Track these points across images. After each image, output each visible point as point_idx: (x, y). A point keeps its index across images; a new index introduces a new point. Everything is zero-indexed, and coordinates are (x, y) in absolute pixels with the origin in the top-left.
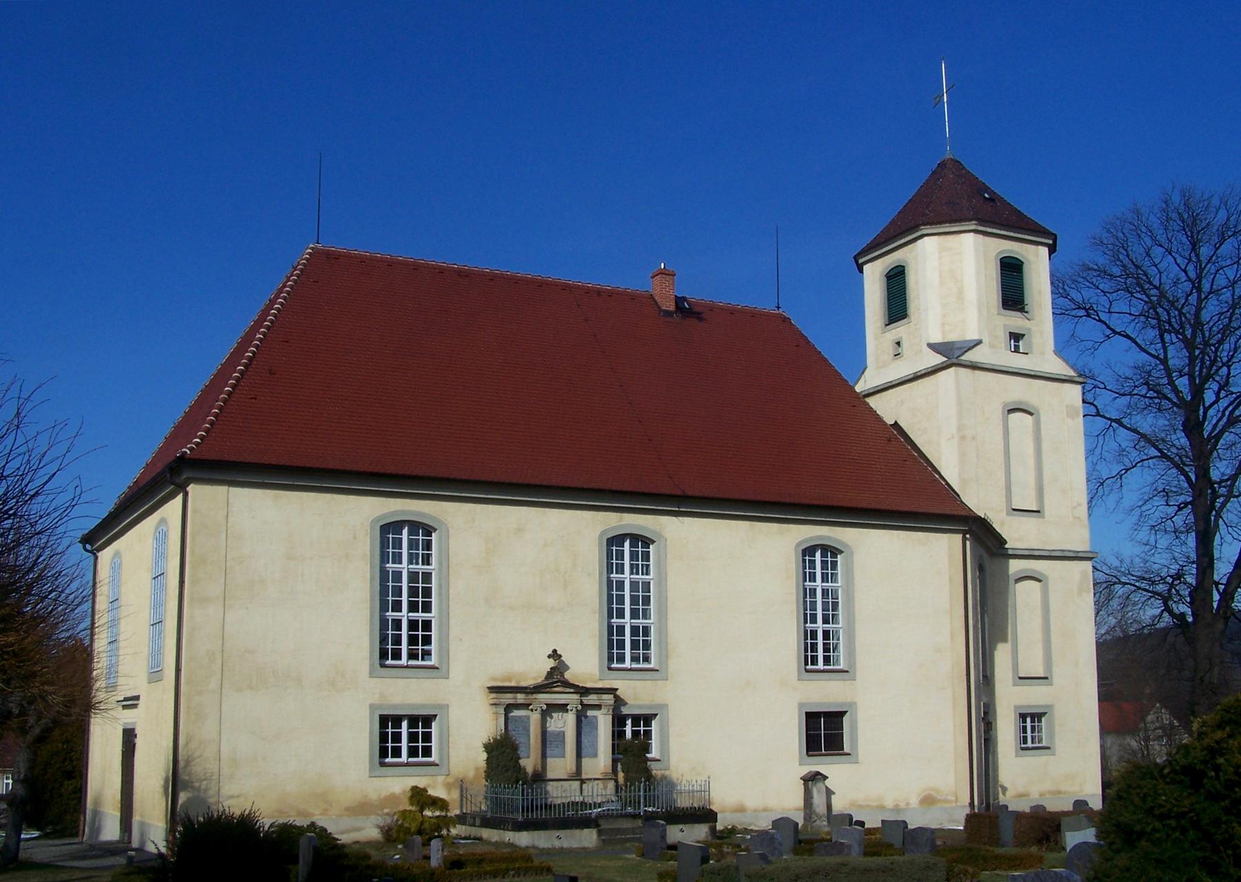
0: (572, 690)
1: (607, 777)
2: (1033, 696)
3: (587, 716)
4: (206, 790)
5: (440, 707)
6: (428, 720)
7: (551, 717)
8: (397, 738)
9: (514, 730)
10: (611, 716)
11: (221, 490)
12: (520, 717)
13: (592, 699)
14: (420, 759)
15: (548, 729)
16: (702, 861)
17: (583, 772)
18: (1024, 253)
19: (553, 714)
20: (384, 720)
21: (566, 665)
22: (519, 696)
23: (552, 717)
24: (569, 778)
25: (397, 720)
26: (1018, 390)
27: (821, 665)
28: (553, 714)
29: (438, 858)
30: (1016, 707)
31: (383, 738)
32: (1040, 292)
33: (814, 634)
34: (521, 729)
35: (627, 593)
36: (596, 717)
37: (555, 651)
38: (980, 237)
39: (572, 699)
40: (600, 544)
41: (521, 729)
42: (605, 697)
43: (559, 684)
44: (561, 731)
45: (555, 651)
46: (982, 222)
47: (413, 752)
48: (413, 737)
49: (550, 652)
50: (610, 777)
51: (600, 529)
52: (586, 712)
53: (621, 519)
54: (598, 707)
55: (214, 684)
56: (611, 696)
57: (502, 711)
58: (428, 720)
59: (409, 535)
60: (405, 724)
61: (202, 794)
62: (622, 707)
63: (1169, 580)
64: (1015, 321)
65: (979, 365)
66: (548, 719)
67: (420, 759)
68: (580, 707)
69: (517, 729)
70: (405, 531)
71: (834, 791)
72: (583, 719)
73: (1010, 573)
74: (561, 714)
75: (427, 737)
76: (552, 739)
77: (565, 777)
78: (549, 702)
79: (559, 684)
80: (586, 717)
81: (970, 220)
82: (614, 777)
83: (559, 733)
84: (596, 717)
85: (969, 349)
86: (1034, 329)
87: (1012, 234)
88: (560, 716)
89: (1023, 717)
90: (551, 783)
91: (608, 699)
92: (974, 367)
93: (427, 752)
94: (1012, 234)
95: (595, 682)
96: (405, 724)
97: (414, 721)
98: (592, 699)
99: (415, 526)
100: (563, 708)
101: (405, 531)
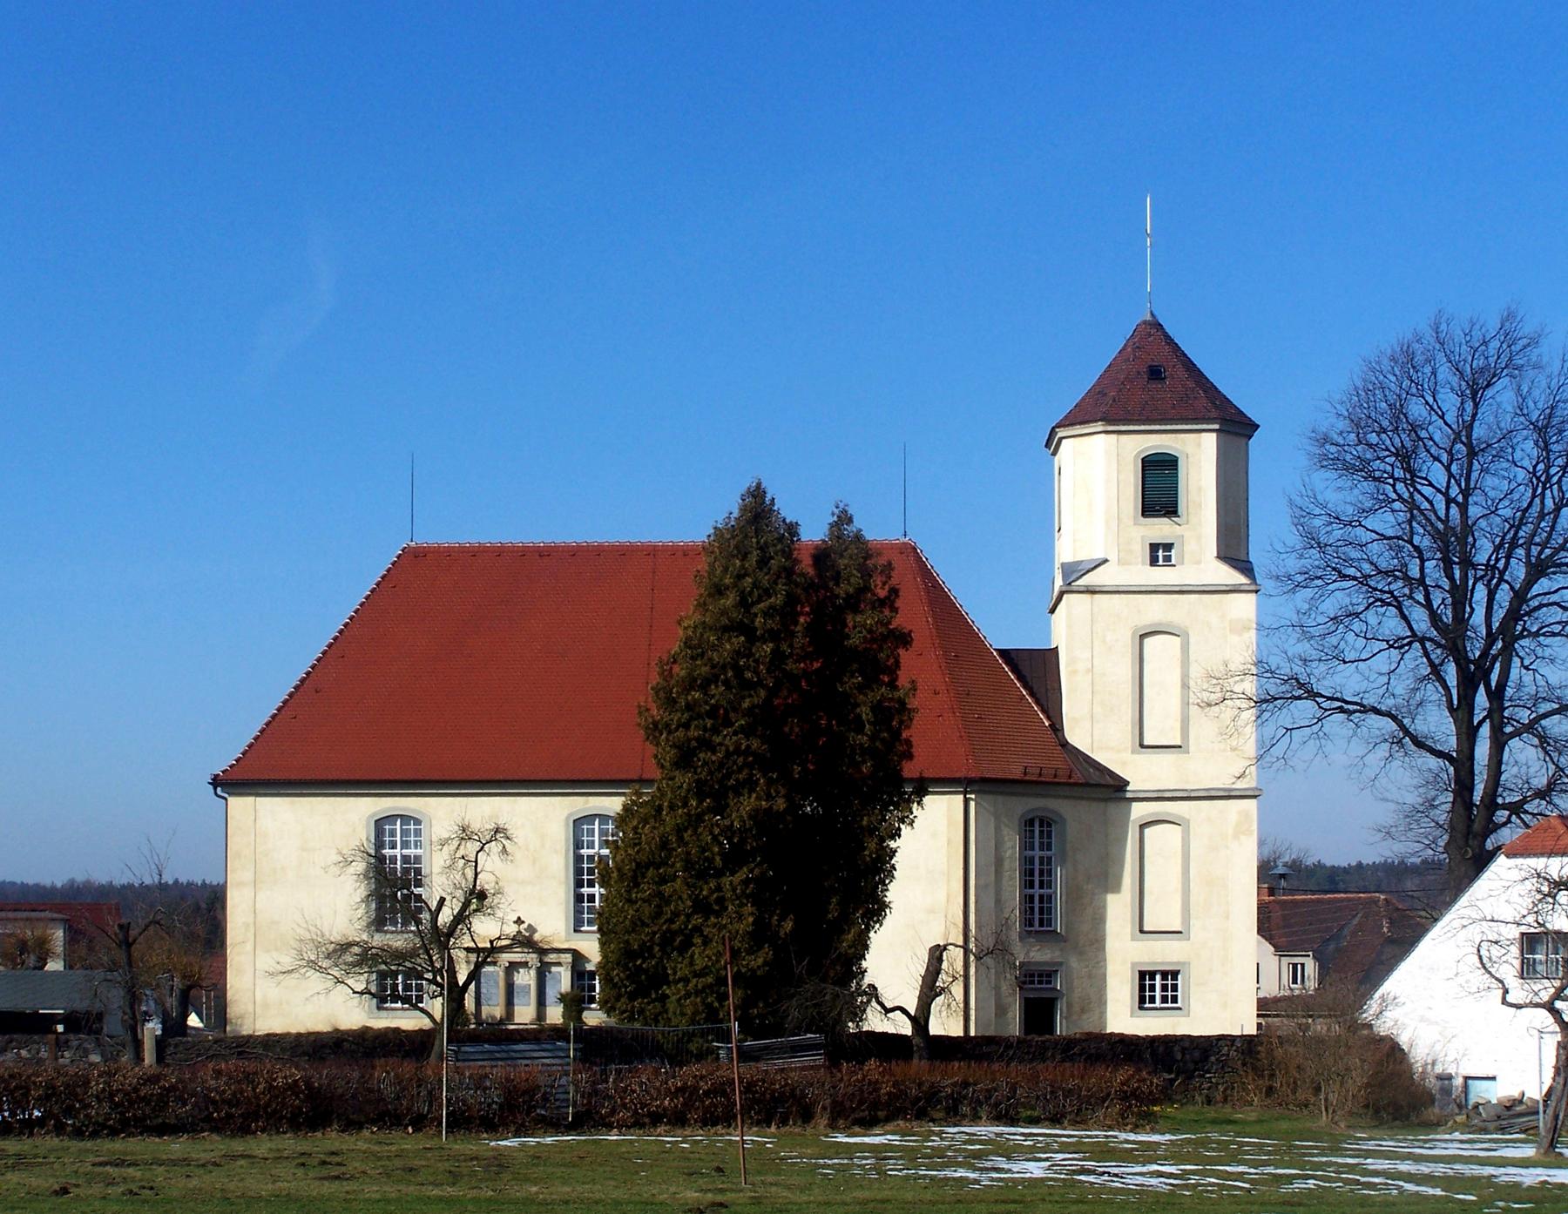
2: (1160, 954)
4: (241, 1026)
5: (1184, 964)
6: (1175, 974)
7: (518, 972)
8: (1152, 988)
11: (251, 799)
13: (552, 958)
14: (1170, 1005)
18: (1178, 446)
20: (1142, 975)
25: (1152, 975)
26: (1155, 610)
27: (1037, 927)
30: (1133, 965)
31: (1142, 988)
32: (1200, 489)
33: (1032, 897)
35: (1037, 867)
36: (560, 973)
37: (519, 918)
38: (1114, 437)
39: (532, 958)
40: (567, 825)
45: (519, 918)
46: (1108, 420)
47: (1164, 999)
48: (1164, 988)
49: (522, 919)
51: (566, 813)
53: (587, 802)
54: (559, 964)
55: (249, 947)
58: (1175, 974)
59: (600, 825)
60: (1158, 977)
61: (238, 1028)
63: (1501, 815)
64: (1160, 529)
65: (1098, 589)
66: (516, 974)
67: (1170, 1005)
68: (539, 965)
70: (597, 822)
73: (1132, 818)
75: (1175, 988)
78: (511, 960)
81: (1096, 421)
84: (560, 973)
85: (1088, 571)
86: (1187, 534)
87: (1143, 428)
89: (1142, 975)
91: (568, 958)
92: (1091, 591)
93: (1175, 1000)
94: (1143, 428)
95: (562, 943)
96: (1158, 977)
97: (1165, 975)
98: (552, 958)
99: (405, 819)
100: (525, 964)
101: (597, 822)
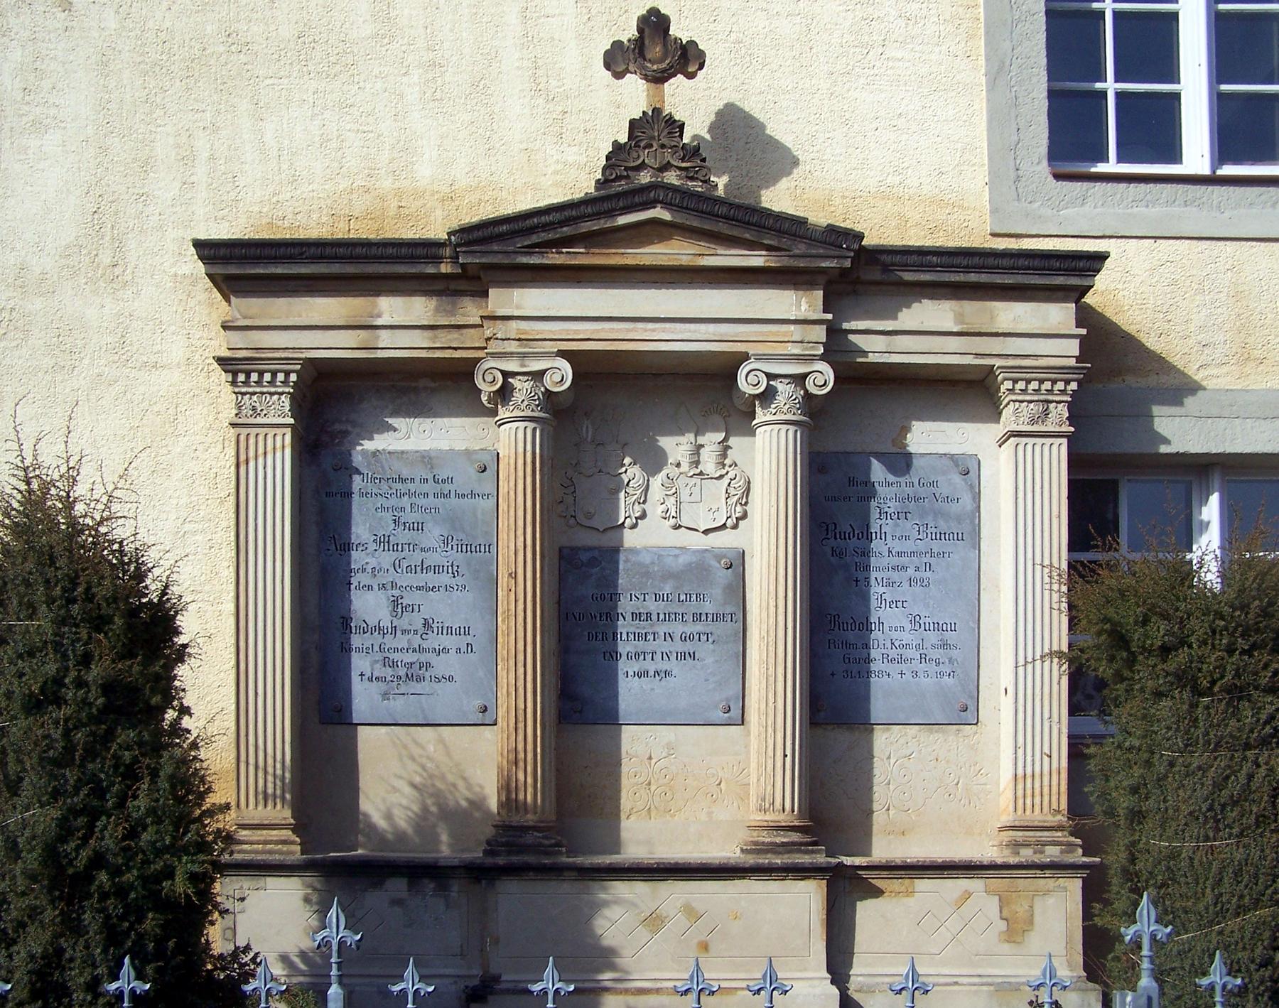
0: (757, 259)
1: (1027, 855)
3: (908, 457)
9: (384, 542)
10: (1060, 450)
12: (426, 459)
15: (630, 539)
16: (1218, 76)
17: (879, 818)
19: (666, 442)
21: (774, 146)
22: (391, 308)
23: (654, 461)
24: (751, 860)
28: (666, 442)
29: (467, 987)
34: (433, 534)
36: (967, 468)
37: (655, 24)
41: (433, 534)
42: (1011, 314)
43: (659, 213)
44: (718, 554)
45: (655, 24)
50: (1052, 853)
52: (906, 429)
56: (1059, 315)
57: (279, 410)
62: (1156, 410)
69: (403, 536)
71: (1169, 437)
72: (878, 472)
74: (712, 439)
76: (652, 606)
77: (728, 851)
79: (659, 213)
80: (901, 462)
82: (1078, 857)
83: (699, 568)
88: (709, 463)
90: (622, 889)
